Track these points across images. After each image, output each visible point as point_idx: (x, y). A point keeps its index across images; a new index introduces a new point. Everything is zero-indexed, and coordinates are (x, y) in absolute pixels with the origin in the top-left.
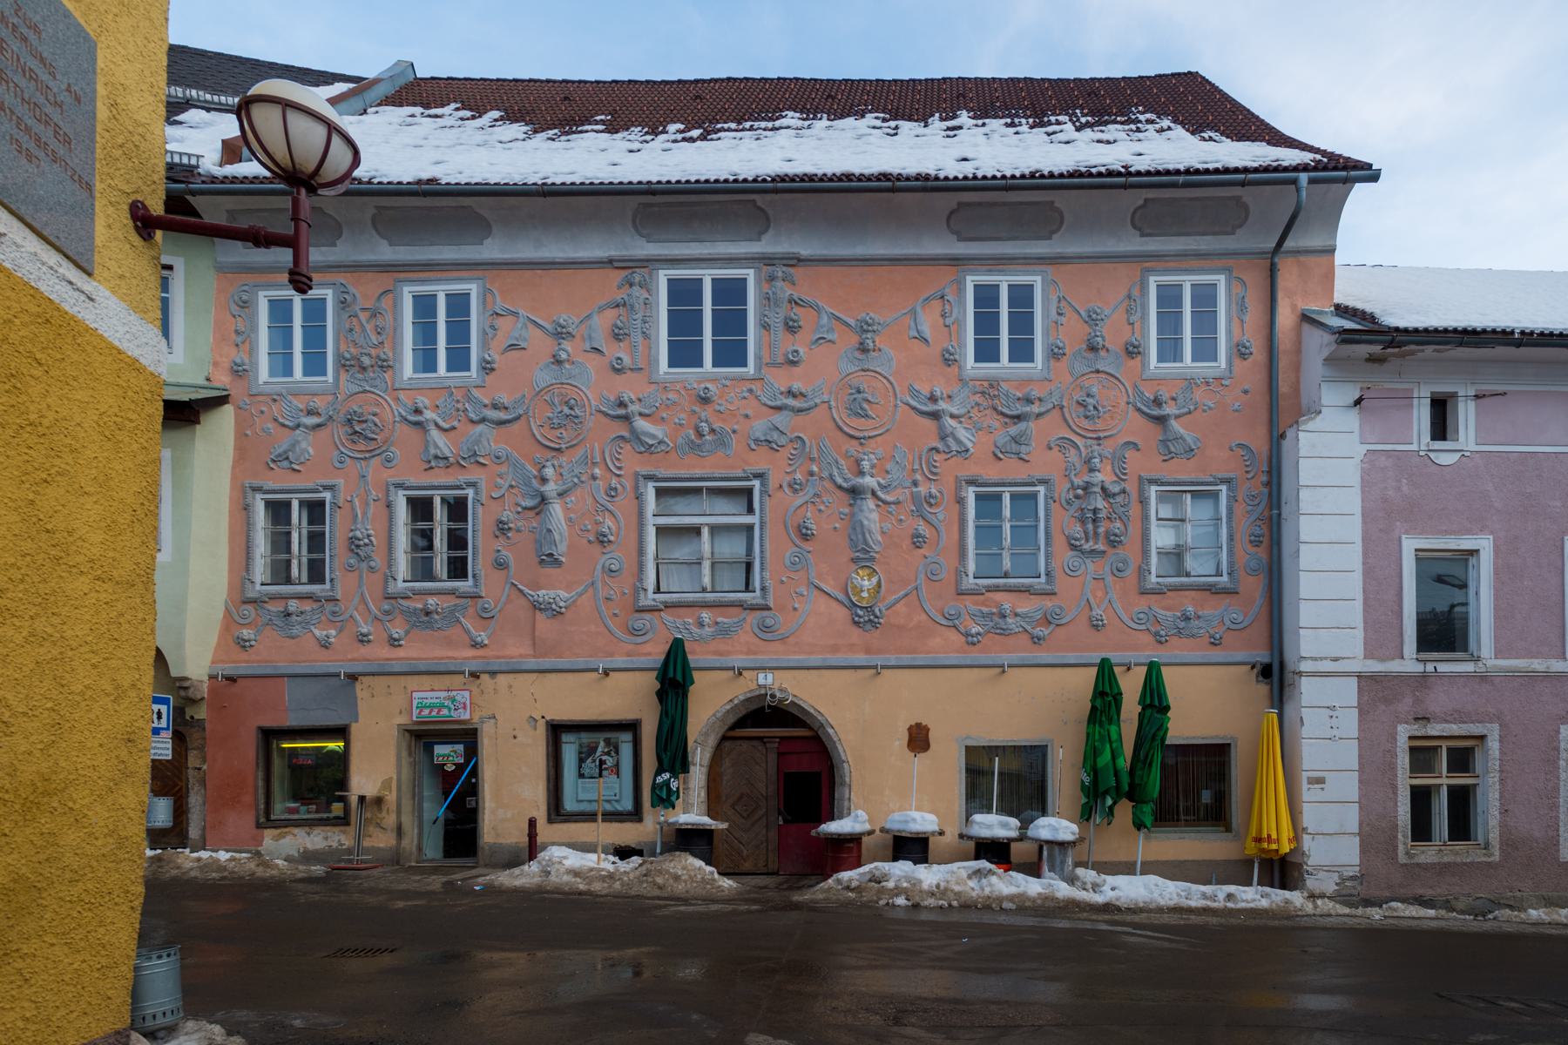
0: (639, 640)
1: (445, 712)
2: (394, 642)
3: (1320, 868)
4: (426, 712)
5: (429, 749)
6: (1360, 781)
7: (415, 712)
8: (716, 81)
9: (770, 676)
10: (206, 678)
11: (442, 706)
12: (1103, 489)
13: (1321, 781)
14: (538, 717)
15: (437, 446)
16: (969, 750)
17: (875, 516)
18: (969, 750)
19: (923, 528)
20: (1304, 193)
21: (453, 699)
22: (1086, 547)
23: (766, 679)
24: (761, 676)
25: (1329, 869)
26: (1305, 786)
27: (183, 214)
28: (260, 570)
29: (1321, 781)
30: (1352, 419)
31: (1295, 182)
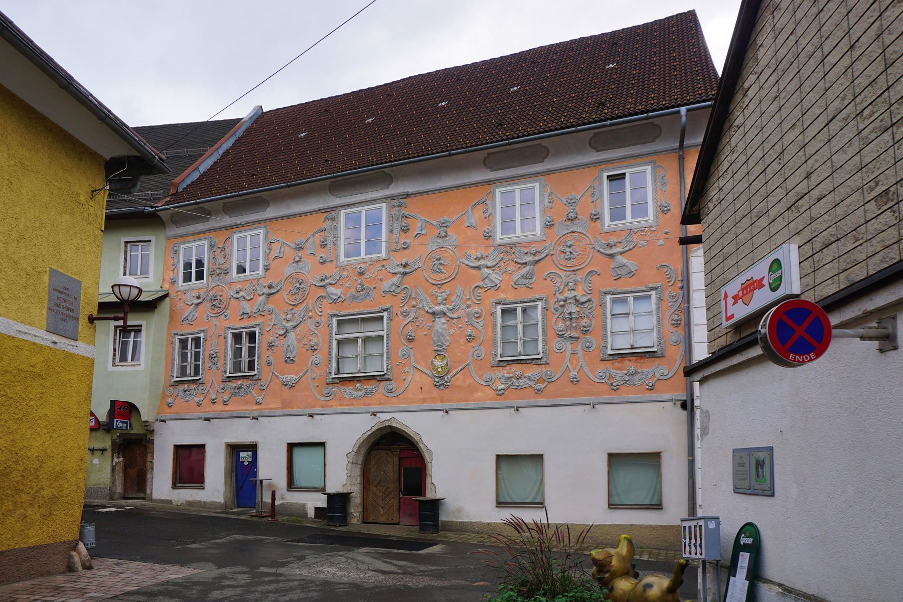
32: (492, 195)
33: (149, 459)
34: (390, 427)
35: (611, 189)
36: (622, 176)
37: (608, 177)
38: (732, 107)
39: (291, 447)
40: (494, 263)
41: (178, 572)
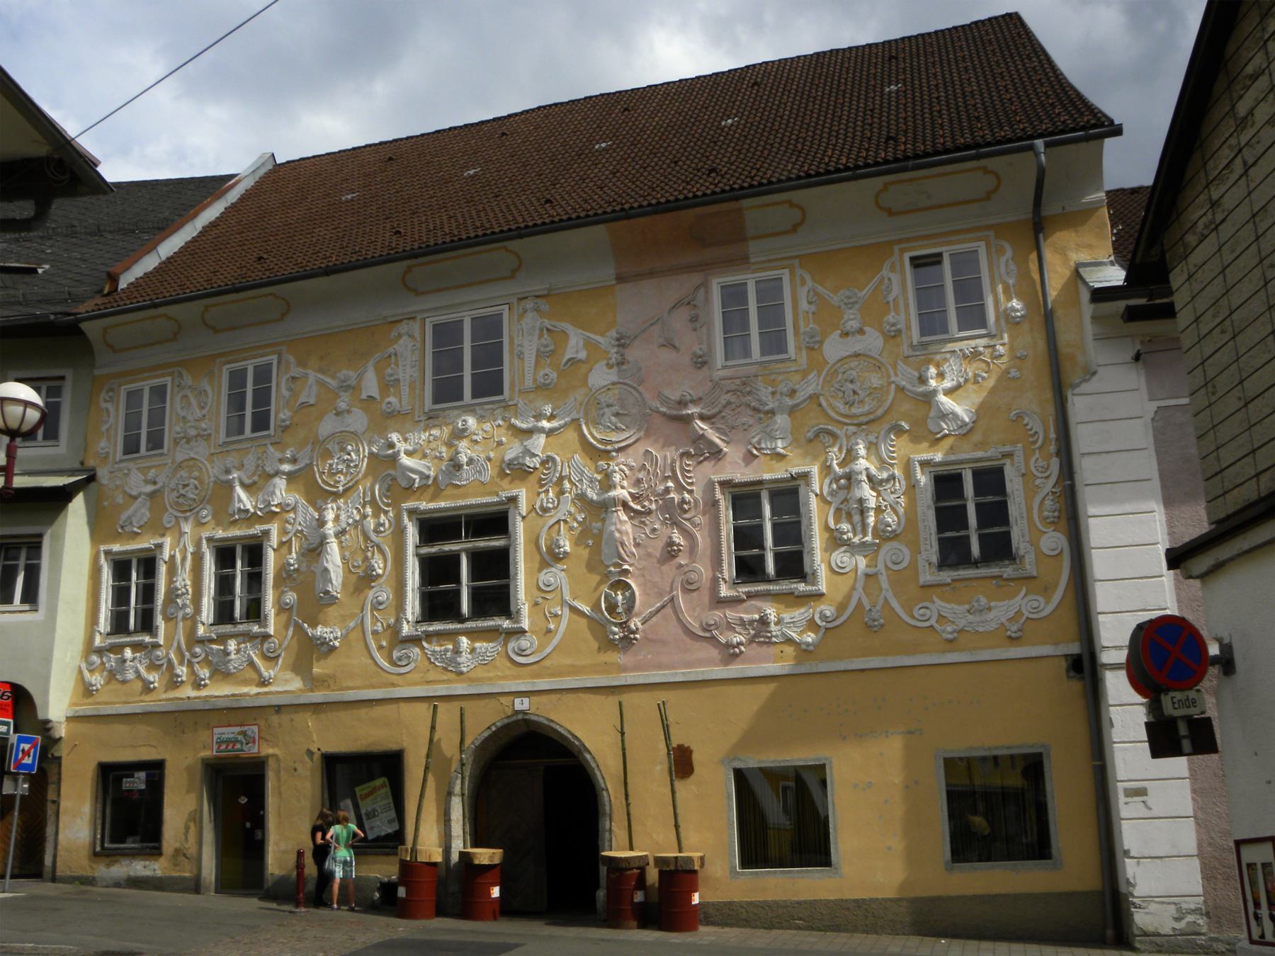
0: (403, 670)
1: (238, 746)
2: (198, 685)
3: (1149, 898)
4: (223, 747)
5: (118, 781)
6: (1194, 791)
7: (215, 747)
8: (527, 111)
9: (526, 700)
10: (63, 719)
11: (236, 741)
12: (870, 478)
13: (1141, 792)
14: (315, 750)
15: (240, 500)
16: (950, 763)
17: (628, 527)
18: (950, 763)
19: (677, 538)
20: (1043, 157)
21: (244, 733)
22: (856, 540)
23: (522, 704)
24: (517, 701)
25: (1165, 899)
26: (1122, 799)
27: (165, 229)
28: (104, 624)
29: (1141, 792)
30: (1134, 378)
31: (1031, 148)
32: (705, 285)
33: (51, 795)
34: (525, 721)
35: (917, 280)
36: (936, 260)
37: (912, 259)
38: (1231, 48)
39: (1238, 843)
40: (716, 410)
41: (771, 471)
